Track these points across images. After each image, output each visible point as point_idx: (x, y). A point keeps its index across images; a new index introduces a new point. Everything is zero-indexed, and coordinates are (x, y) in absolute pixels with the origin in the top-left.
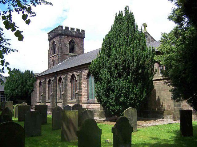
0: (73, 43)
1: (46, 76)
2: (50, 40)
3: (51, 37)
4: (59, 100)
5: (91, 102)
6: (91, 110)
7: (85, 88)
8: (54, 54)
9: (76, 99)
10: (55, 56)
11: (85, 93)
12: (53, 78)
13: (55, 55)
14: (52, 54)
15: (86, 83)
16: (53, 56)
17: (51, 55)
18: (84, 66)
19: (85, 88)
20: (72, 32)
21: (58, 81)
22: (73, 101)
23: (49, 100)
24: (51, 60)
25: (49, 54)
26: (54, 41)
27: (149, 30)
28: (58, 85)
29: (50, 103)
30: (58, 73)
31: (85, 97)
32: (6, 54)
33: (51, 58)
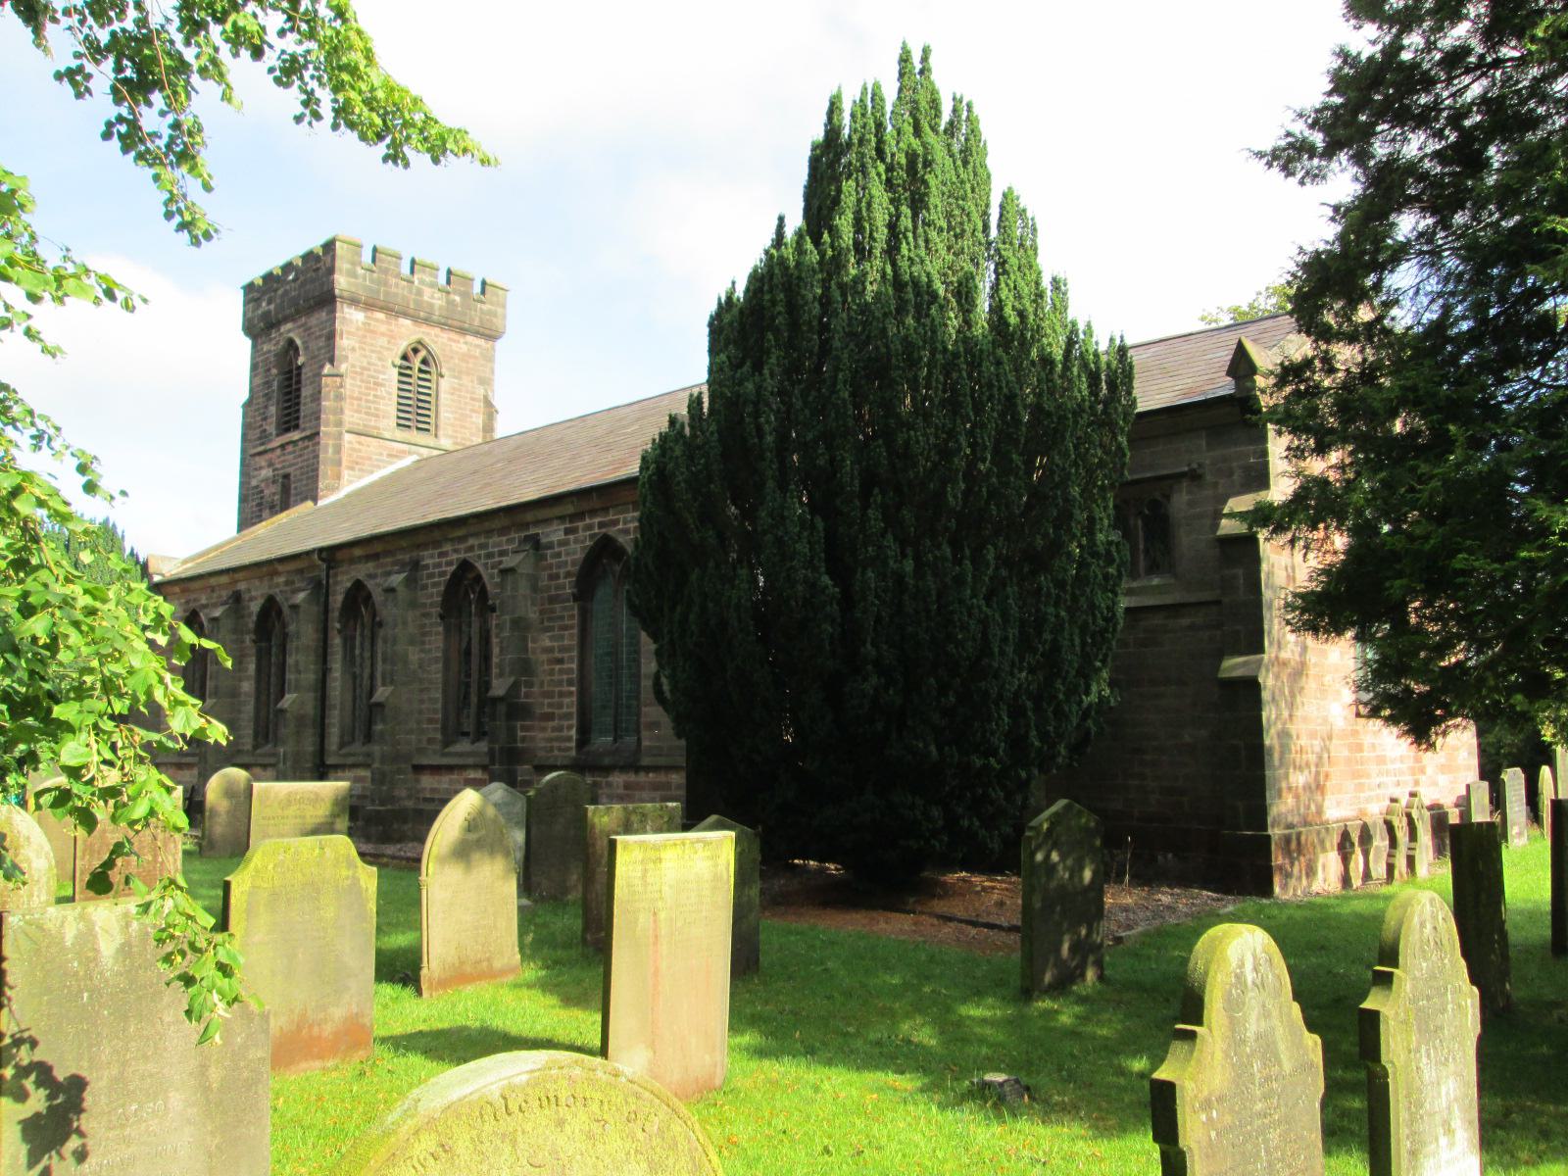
0: (424, 362)
1: (239, 575)
2: (258, 327)
3: (266, 315)
4: (342, 745)
5: (607, 761)
6: (1319, 900)
7: (560, 661)
8: (287, 430)
9: (480, 734)
10: (294, 443)
11: (561, 694)
12: (1528, 322)
13: (295, 435)
14: (271, 428)
15: (564, 628)
16: (283, 447)
17: (264, 437)
18: (558, 511)
19: (560, 661)
20: (420, 293)
21: (336, 614)
22: (461, 755)
23: (256, 747)
24: (267, 473)
25: (247, 427)
26: (291, 343)
27: (1352, 193)
28: (336, 641)
29: (1346, 881)
30: (339, 555)
31: (556, 723)
32: (82, 50)
33: (262, 461)
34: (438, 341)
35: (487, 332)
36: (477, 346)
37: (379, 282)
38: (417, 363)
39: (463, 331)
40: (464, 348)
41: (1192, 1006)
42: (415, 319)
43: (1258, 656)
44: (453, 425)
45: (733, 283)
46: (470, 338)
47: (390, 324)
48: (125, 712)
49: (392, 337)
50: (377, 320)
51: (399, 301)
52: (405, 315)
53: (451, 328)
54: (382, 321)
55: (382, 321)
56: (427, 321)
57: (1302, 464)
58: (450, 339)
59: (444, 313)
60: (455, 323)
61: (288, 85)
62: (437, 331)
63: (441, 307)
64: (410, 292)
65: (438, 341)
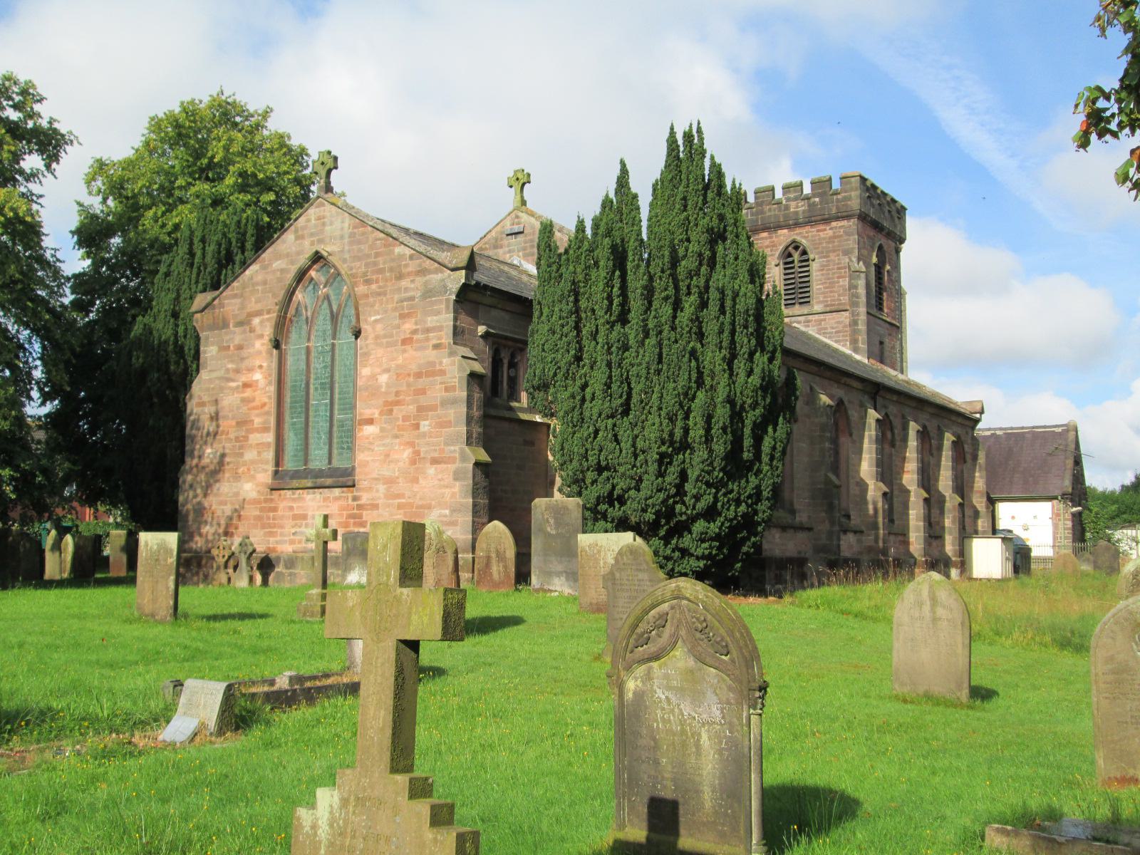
34: (804, 236)
35: (845, 214)
36: (841, 227)
37: (757, 213)
38: (796, 256)
39: (827, 220)
40: (830, 233)
41: (80, 244)
42: (788, 227)
43: (672, 839)
44: (824, 293)
45: (55, 177)
46: (834, 224)
47: (771, 238)
48: (843, 537)
49: (773, 246)
50: (762, 238)
51: (773, 220)
52: (780, 227)
53: (817, 222)
54: (766, 238)
55: (766, 238)
56: (797, 225)
57: (381, 401)
58: (818, 231)
59: (807, 215)
60: (819, 218)
61: (26, 83)
62: (808, 228)
63: (804, 212)
64: (780, 210)
65: (804, 236)
